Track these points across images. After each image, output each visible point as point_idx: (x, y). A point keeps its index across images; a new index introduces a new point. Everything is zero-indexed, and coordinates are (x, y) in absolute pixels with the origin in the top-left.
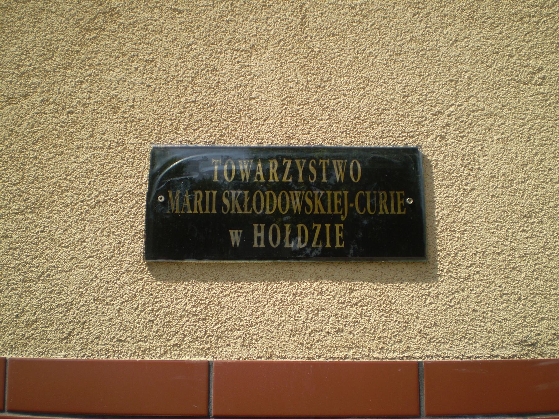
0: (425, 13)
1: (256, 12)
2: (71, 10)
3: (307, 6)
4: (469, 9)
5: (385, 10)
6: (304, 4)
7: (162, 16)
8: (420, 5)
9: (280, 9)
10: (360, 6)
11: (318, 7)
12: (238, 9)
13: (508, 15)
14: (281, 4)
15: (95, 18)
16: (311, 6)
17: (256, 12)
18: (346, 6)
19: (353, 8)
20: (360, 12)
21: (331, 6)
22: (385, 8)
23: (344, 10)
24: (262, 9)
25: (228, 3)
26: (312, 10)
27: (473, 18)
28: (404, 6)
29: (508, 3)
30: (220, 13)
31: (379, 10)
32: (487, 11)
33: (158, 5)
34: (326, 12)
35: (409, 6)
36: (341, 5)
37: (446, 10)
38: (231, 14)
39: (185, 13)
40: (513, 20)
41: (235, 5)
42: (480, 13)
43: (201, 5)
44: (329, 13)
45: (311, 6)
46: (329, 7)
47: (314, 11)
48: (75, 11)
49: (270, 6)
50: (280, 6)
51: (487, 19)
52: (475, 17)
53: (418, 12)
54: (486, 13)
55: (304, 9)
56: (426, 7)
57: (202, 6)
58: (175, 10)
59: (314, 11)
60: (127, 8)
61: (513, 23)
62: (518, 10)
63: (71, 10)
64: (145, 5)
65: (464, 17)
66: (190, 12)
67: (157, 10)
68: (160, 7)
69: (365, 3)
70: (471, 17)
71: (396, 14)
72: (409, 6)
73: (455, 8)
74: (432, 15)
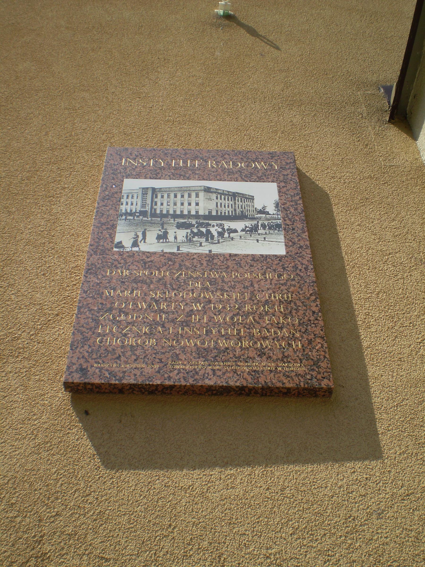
0: (335, 560)
1: (178, 562)
2: (5, 552)
3: (225, 556)
4: (376, 553)
5: (298, 559)
6: (222, 554)
7: (90, 564)
8: (330, 552)
9: (200, 559)
10: (274, 555)
11: (235, 557)
12: (160, 559)
13: (412, 557)
14: (201, 554)
15: (27, 562)
16: (229, 556)
17: (178, 562)
18: (262, 556)
19: (268, 557)
20: (274, 562)
21: (247, 556)
22: (298, 557)
23: (260, 559)
24: (183, 559)
25: (152, 552)
26: (230, 561)
27: (380, 562)
28: (315, 554)
29: (411, 545)
30: (144, 562)
31: (292, 559)
32: (392, 554)
33: (87, 552)
34: (242, 562)
35: (320, 554)
36: (257, 555)
37: (354, 556)
38: (154, 563)
39: (111, 561)
40: (417, 562)
41: (158, 555)
42: (386, 557)
43: (127, 554)
44: (245, 563)
45: (229, 556)
46: (246, 557)
47: (232, 562)
48: (8, 554)
49: (190, 556)
50: (200, 556)
51: (392, 562)
52: (382, 561)
53: (328, 559)
54: (391, 557)
55: (222, 559)
56: (336, 554)
57: (127, 555)
58: (102, 558)
59: (232, 562)
60: (58, 554)
61: (417, 564)
62: (421, 551)
63: (5, 552)
64: (75, 552)
65: (371, 562)
66: (116, 560)
67: (85, 557)
68: (88, 554)
69: (279, 553)
70: (378, 562)
71: (308, 562)
72: (320, 554)
73: (362, 554)
74: (341, 562)
